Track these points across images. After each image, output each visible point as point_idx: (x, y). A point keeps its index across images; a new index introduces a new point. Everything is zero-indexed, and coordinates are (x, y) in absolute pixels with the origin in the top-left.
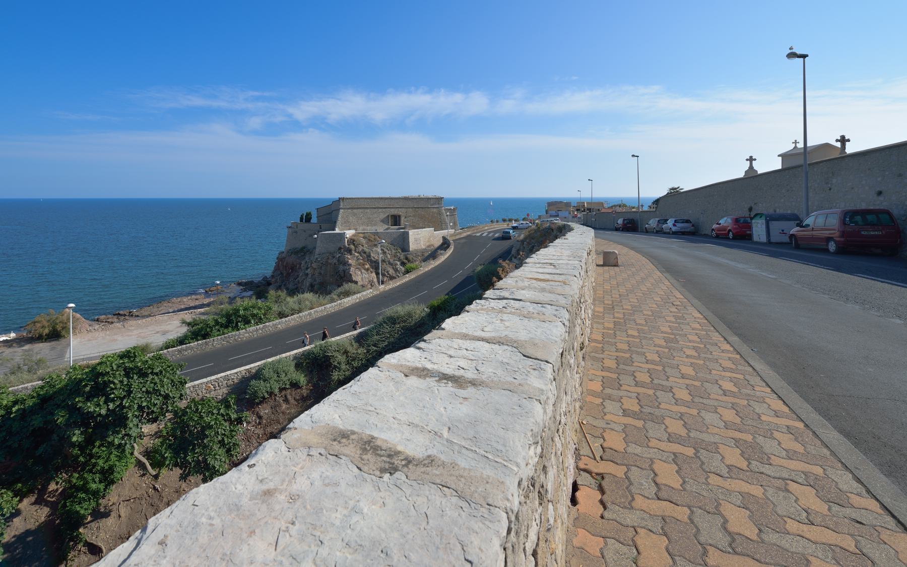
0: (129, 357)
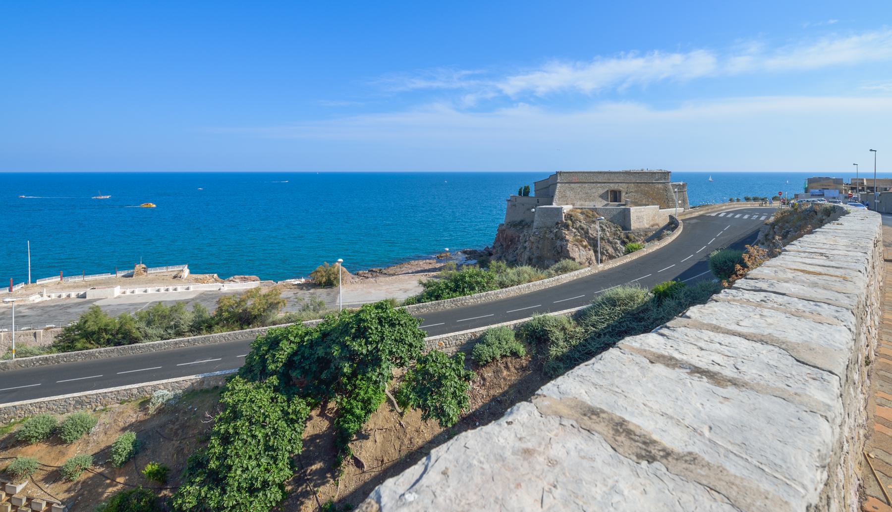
0: (382, 308)
